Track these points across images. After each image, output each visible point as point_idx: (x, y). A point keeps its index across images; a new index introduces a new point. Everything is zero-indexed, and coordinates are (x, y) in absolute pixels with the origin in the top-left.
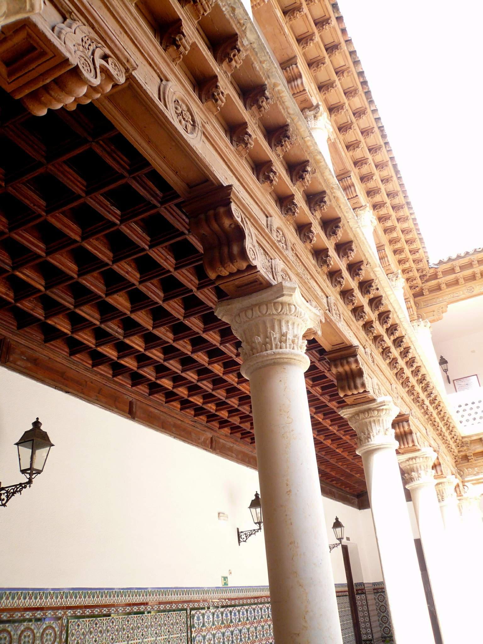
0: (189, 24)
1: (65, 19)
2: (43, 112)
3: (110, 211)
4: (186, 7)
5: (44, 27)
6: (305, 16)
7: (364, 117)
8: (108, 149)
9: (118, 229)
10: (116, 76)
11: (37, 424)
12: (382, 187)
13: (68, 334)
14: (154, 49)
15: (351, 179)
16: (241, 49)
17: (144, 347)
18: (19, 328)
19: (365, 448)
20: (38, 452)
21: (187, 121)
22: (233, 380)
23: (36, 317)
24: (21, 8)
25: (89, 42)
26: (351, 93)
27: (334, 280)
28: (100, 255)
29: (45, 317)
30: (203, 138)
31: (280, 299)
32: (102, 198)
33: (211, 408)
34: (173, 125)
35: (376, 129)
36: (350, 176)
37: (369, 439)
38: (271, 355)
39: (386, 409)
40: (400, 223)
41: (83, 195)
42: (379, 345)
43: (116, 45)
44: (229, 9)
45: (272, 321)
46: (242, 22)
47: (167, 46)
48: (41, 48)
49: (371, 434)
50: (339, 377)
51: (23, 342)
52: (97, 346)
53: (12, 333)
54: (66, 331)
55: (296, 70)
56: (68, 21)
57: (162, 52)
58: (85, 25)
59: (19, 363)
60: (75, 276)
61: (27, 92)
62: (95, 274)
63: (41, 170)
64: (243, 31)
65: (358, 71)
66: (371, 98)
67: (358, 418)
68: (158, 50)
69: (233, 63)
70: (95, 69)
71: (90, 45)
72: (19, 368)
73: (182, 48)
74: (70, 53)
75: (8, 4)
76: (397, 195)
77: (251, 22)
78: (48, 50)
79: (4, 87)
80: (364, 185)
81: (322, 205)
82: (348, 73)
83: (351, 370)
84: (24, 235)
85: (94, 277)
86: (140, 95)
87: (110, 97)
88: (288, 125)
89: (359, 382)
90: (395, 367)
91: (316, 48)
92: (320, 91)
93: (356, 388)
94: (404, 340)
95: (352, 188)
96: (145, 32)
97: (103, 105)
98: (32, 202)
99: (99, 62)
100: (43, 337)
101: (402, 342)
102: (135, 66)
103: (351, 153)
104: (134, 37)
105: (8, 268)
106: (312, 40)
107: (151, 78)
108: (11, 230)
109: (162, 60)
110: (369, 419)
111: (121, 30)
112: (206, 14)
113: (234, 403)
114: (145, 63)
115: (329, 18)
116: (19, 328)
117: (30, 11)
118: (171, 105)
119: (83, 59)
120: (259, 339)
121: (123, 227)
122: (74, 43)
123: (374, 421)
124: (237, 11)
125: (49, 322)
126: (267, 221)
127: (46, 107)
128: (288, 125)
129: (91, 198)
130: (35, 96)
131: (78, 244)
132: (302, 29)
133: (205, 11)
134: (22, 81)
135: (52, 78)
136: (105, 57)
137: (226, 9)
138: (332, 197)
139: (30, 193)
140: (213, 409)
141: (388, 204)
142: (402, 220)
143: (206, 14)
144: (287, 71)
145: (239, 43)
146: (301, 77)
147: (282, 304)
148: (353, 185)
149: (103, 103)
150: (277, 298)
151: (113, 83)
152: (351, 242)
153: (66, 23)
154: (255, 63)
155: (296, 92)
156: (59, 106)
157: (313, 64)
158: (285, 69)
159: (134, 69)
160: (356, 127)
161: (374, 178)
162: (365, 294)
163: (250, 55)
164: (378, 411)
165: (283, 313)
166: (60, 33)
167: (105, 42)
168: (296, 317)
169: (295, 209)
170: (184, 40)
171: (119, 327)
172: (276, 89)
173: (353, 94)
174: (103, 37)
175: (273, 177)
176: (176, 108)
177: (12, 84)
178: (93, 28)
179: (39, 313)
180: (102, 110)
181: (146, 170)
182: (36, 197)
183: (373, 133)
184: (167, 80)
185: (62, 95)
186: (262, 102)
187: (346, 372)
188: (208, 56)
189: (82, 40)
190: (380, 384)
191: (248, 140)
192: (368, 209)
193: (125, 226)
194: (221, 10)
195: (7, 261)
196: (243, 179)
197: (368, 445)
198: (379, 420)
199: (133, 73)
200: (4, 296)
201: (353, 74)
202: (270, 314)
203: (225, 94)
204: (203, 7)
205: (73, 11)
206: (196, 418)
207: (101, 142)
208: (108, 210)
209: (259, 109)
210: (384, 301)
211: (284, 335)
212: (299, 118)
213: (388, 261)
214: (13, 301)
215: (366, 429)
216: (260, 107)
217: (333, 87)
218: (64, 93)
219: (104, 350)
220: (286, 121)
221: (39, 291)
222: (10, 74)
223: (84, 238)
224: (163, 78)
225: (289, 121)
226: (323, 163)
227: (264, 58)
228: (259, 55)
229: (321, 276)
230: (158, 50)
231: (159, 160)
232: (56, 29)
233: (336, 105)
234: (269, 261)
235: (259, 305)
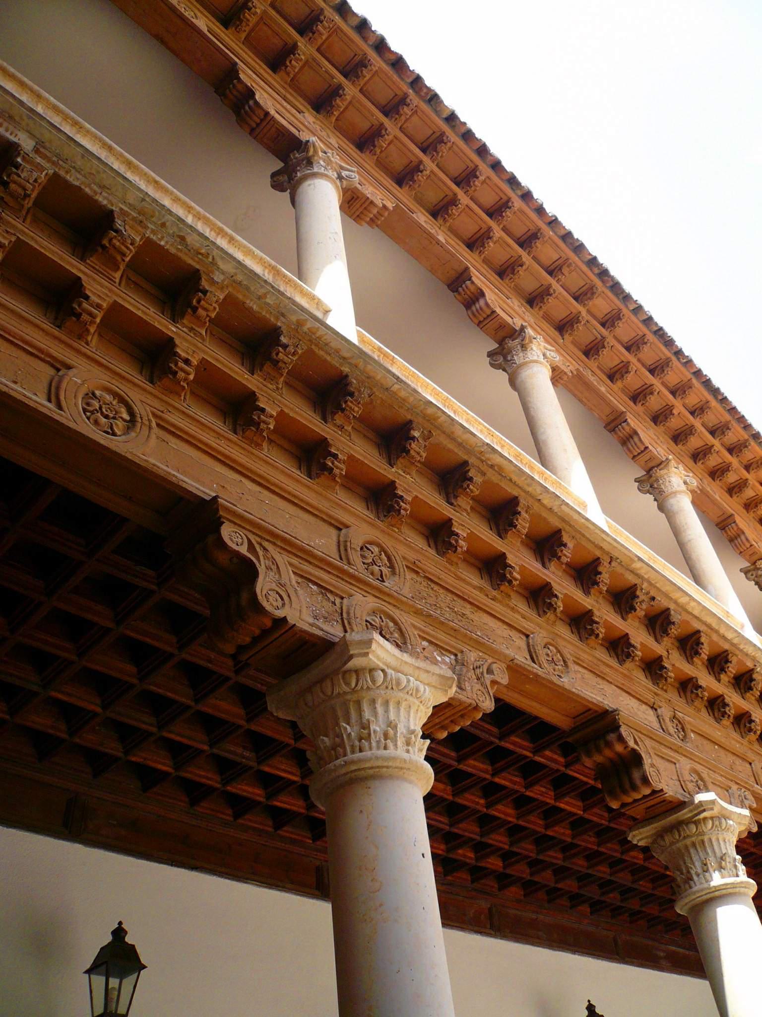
6: (467, 209)
7: (620, 325)
11: (119, 933)
12: (697, 423)
15: (628, 424)
17: (299, 773)
19: (686, 900)
20: (125, 981)
22: (478, 803)
26: (586, 294)
27: (540, 603)
30: (162, 433)
31: (351, 664)
33: (465, 856)
35: (650, 337)
36: (626, 421)
37: (692, 882)
38: (342, 766)
39: (712, 818)
40: (752, 472)
42: (693, 696)
45: (345, 705)
46: (203, 251)
49: (693, 872)
50: (602, 772)
52: (224, 785)
55: (472, 288)
65: (586, 260)
66: (623, 291)
67: (662, 843)
68: (43, 330)
69: (201, 312)
76: (728, 428)
80: (661, 428)
81: (465, 486)
82: (568, 266)
83: (619, 755)
88: (347, 376)
89: (636, 775)
90: (750, 730)
91: (502, 245)
92: (532, 306)
93: (635, 788)
94: (754, 676)
95: (636, 439)
101: (752, 680)
103: (619, 384)
106: (490, 238)
110: (684, 842)
113: (500, 842)
115: (509, 200)
120: (326, 741)
123: (694, 845)
124: (189, 240)
126: (339, 536)
128: (347, 376)
132: (470, 228)
138: (484, 468)
140: (471, 858)
141: (717, 445)
142: (754, 466)
144: (459, 294)
146: (482, 294)
147: (357, 672)
148: (636, 433)
150: (346, 663)
152: (559, 532)
154: (248, 302)
155: (482, 319)
157: (505, 271)
158: (457, 291)
160: (613, 342)
161: (674, 411)
162: (627, 613)
163: (235, 293)
164: (696, 823)
165: (362, 688)
168: (389, 691)
169: (398, 504)
171: (244, 748)
172: (305, 329)
173: (589, 295)
175: (333, 463)
183: (646, 343)
186: (277, 354)
187: (611, 760)
190: (699, 767)
191: (259, 417)
192: (673, 463)
196: (268, 481)
197: (695, 893)
198: (703, 842)
201: (577, 266)
202: (339, 693)
203: (195, 362)
206: (449, 878)
209: (275, 365)
210: (675, 617)
211: (365, 726)
212: (365, 360)
213: (747, 540)
215: (682, 863)
216: (275, 363)
217: (550, 295)
219: (240, 789)
220: (341, 372)
225: (346, 369)
226: (443, 418)
227: (263, 291)
228: (252, 289)
229: (500, 602)
233: (568, 319)
234: (334, 603)
235: (320, 681)
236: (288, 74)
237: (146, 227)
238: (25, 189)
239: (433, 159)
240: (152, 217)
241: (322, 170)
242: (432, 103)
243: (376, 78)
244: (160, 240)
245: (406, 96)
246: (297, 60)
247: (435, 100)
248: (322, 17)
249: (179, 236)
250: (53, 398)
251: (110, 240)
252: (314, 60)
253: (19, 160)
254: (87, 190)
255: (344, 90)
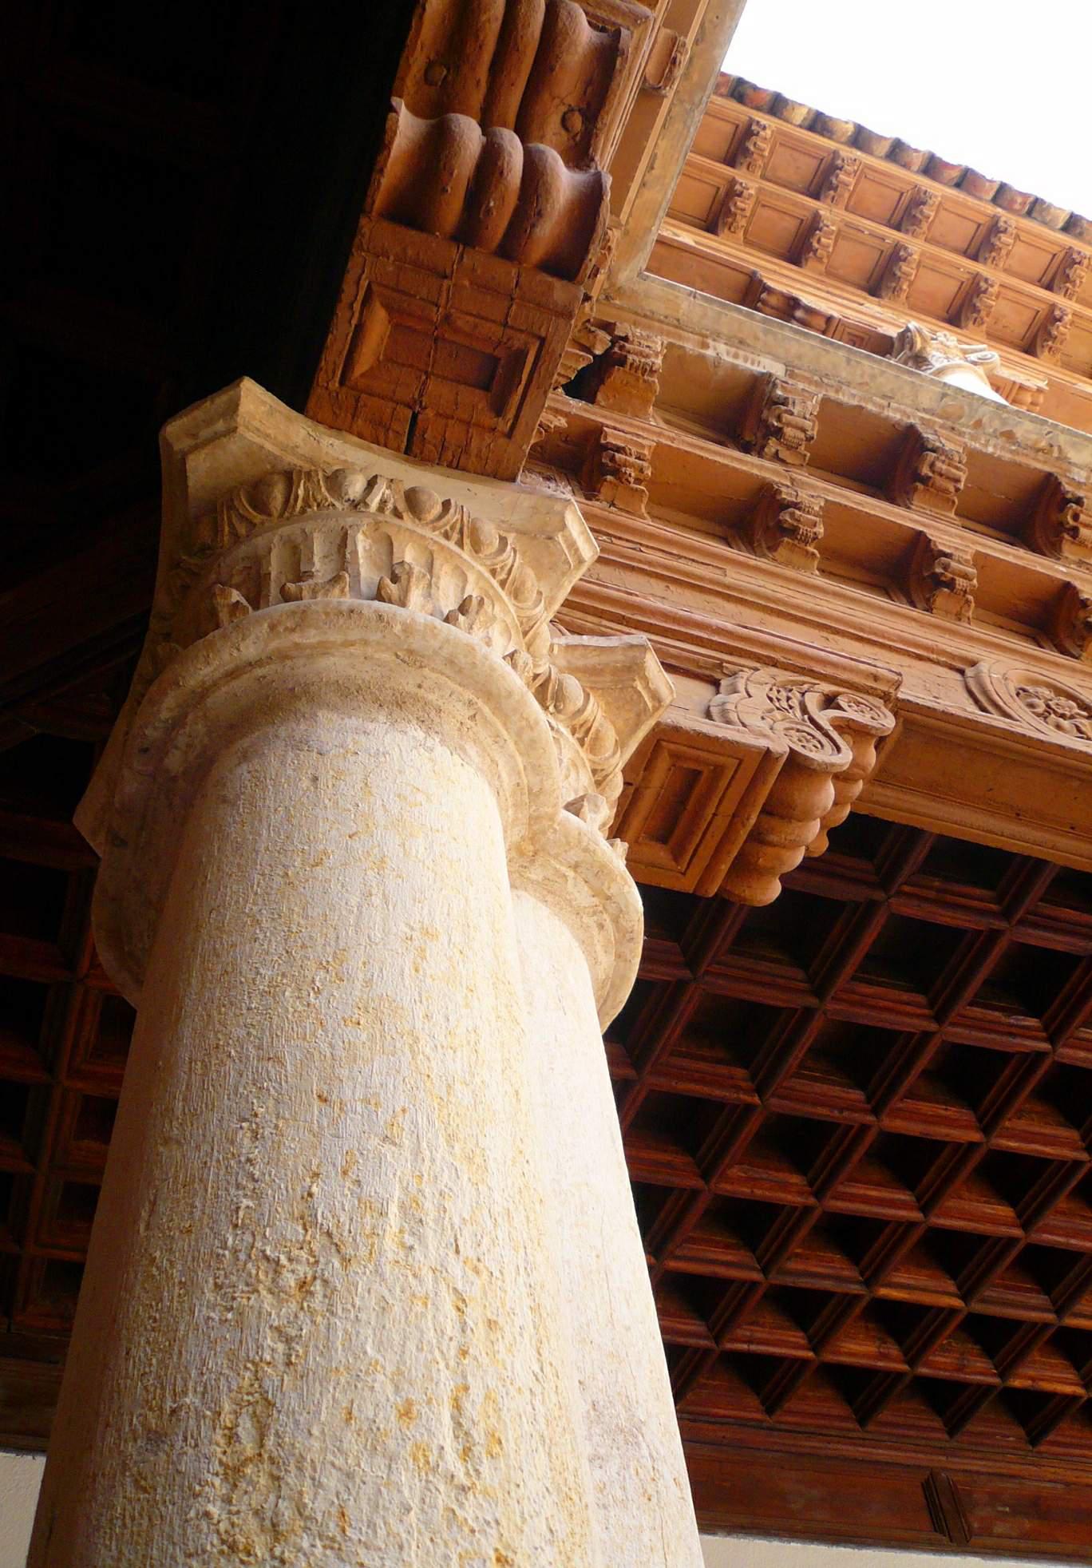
0: (942, 527)
1: (716, 684)
2: (773, 891)
3: (1013, 1030)
4: (916, 502)
5: (693, 722)
8: (932, 894)
9: (1054, 1062)
10: (874, 724)
13: (1081, 1397)
14: (906, 622)
16: (1081, 494)
18: (952, 1430)
21: (1072, 717)
23: (979, 1385)
24: (638, 715)
25: (784, 694)
28: (1048, 1149)
29: (814, 1350)
32: (978, 1012)
34: (1050, 744)
41: (933, 1026)
43: (835, 665)
44: (1001, 441)
46: (1043, 444)
47: (928, 600)
48: (706, 763)
51: (976, 1465)
53: (942, 1451)
54: (1068, 1389)
56: (724, 683)
57: (926, 617)
58: (756, 669)
59: (999, 1528)
60: (1017, 1232)
61: (724, 868)
62: (1061, 1202)
63: (816, 1025)
64: (1058, 459)
68: (914, 620)
70: (827, 735)
71: (788, 699)
72: (1006, 1542)
73: (960, 582)
74: (765, 736)
75: (613, 723)
77: (1063, 431)
78: (721, 760)
79: (678, 887)
84: (854, 1191)
85: (1063, 1213)
86: (939, 730)
87: (881, 777)
96: (869, 605)
97: (877, 803)
98: (832, 1107)
99: (825, 717)
100: (1021, 1432)
102: (896, 678)
104: (855, 628)
105: (855, 1289)
107: (939, 681)
108: (819, 1194)
109: (937, 632)
111: (825, 634)
112: (961, 486)
114: (907, 661)
116: (952, 1430)
117: (656, 709)
118: (1017, 707)
119: (793, 732)
121: (1061, 1050)
122: (760, 713)
124: (1019, 433)
125: (1017, 1383)
127: (774, 875)
129: (953, 1024)
130: (745, 867)
131: (983, 1150)
133: (958, 481)
134: (706, 853)
135: (759, 809)
136: (829, 702)
137: (995, 446)
139: (820, 1088)
143: (961, 486)
145: (1068, 488)
149: (875, 798)
151: (873, 742)
153: (722, 689)
156: (798, 857)
159: (898, 685)
166: (724, 713)
167: (811, 673)
170: (954, 564)
174: (803, 668)
176: (1031, 706)
177: (689, 872)
178: (775, 664)
179: (979, 1370)
180: (881, 813)
181: (1040, 886)
182: (837, 1091)
184: (973, 663)
185: (790, 831)
188: (1022, 558)
189: (771, 699)
193: (1065, 1045)
194: (986, 455)
195: (846, 1273)
199: (900, 696)
200: (881, 1364)
204: (948, 478)
205: (723, 661)
207: (906, 888)
208: (1007, 1030)
214: (811, 1354)
218: (795, 824)
221: (953, 1311)
222: (676, 858)
223: (987, 1129)
224: (960, 666)
230: (914, 620)
231: (1064, 842)
232: (714, 711)
236: (820, 260)
237: (961, 434)
238: (804, 430)
239: (1067, 294)
240: (960, 417)
241: (946, 363)
242: (1034, 214)
243: (943, 213)
244: (986, 445)
245: (995, 220)
246: (828, 235)
247: (1037, 207)
248: (839, 162)
249: (1003, 434)
250: (990, 708)
251: (932, 466)
252: (848, 225)
253: (779, 392)
254: (870, 407)
255: (906, 248)
